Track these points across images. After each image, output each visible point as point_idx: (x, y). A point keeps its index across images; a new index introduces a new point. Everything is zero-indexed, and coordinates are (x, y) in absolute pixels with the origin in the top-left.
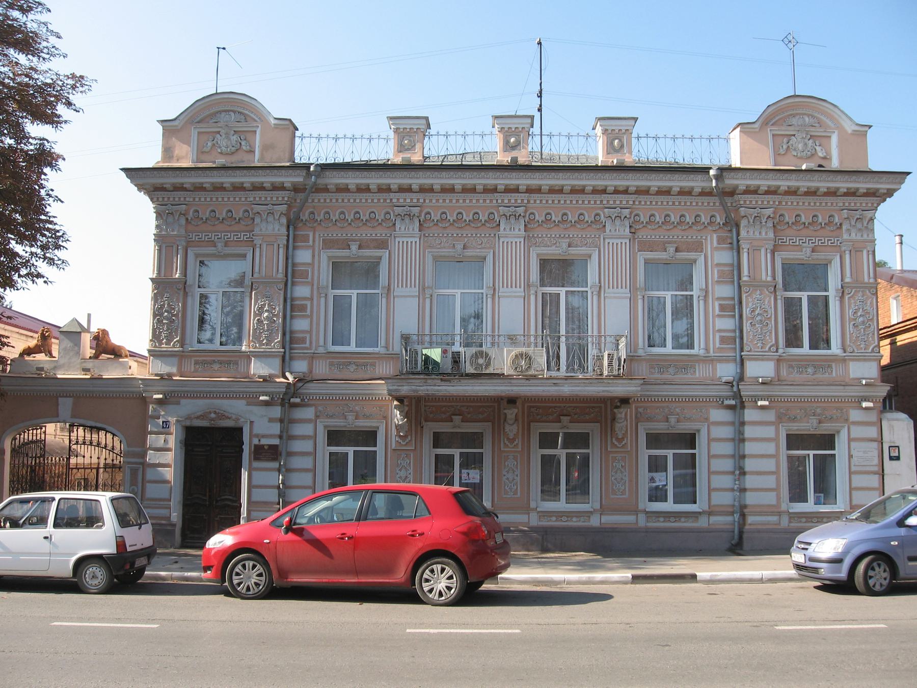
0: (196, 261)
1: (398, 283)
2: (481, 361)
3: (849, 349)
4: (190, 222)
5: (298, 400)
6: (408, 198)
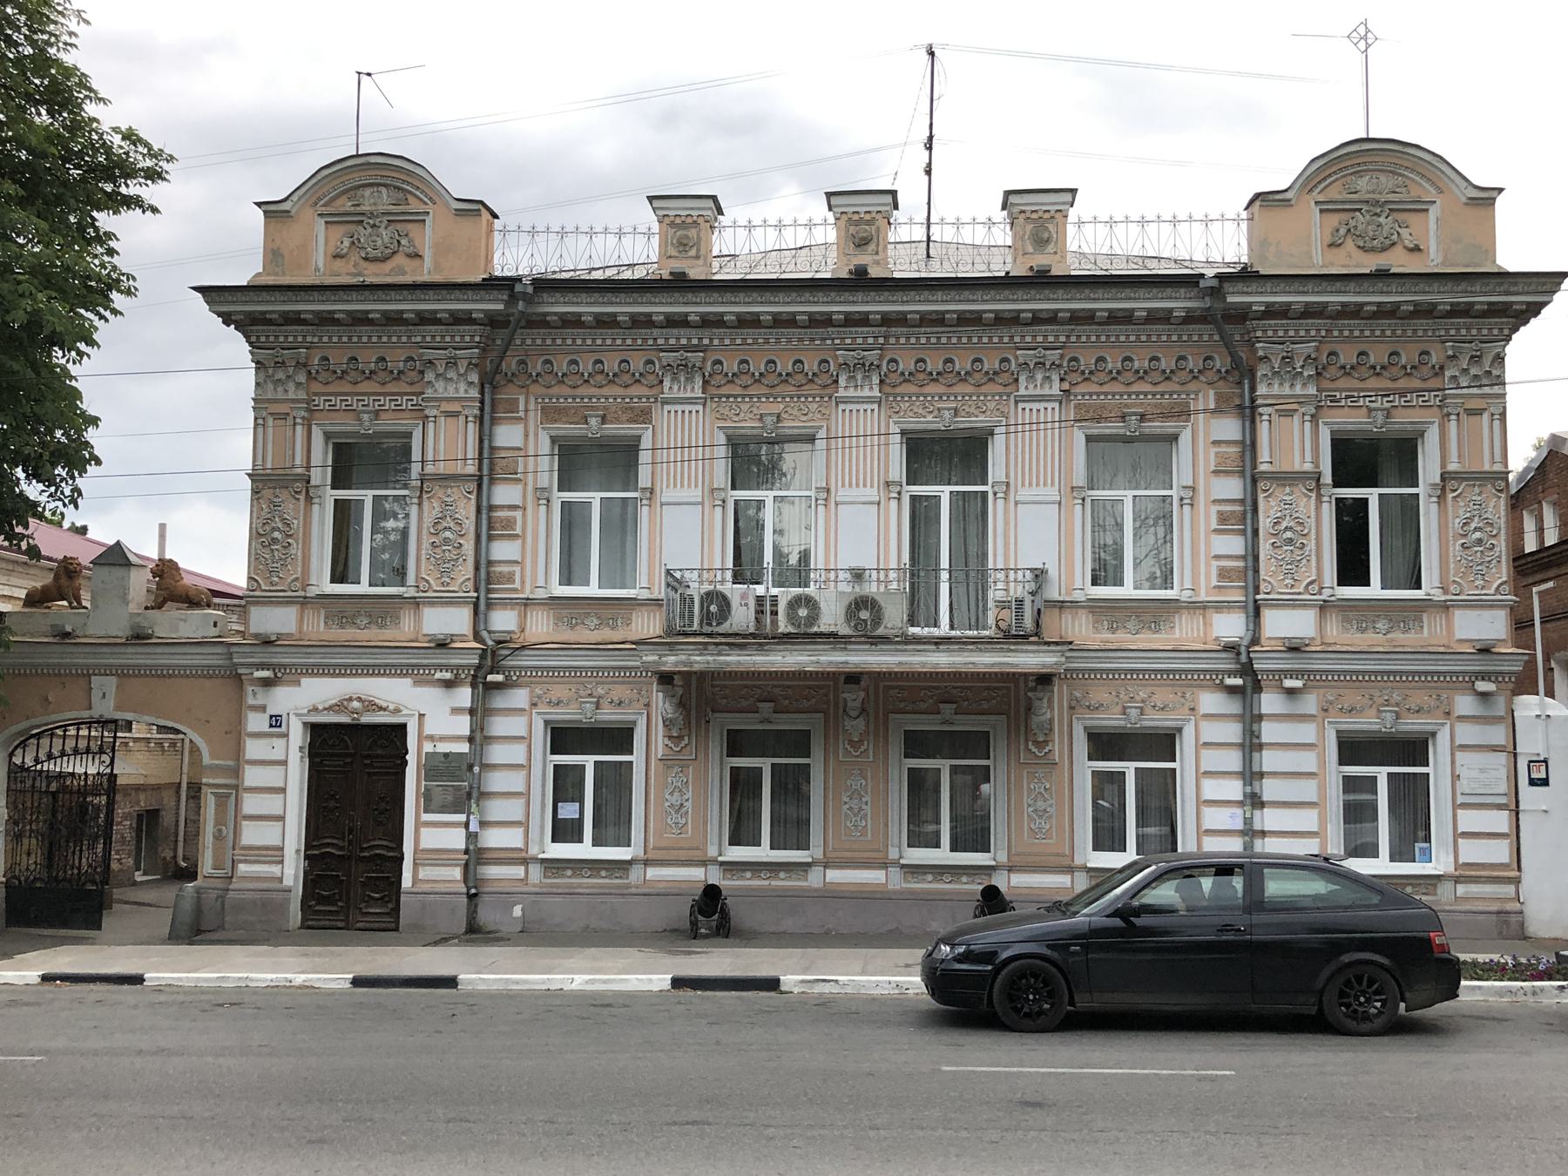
0: (327, 444)
1: (668, 479)
2: (864, 615)
3: (1453, 588)
4: (315, 378)
5: (499, 678)
6: (684, 337)
